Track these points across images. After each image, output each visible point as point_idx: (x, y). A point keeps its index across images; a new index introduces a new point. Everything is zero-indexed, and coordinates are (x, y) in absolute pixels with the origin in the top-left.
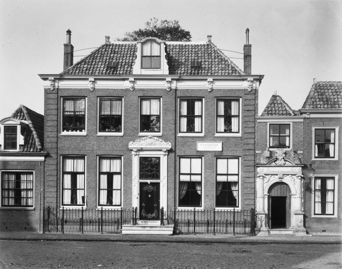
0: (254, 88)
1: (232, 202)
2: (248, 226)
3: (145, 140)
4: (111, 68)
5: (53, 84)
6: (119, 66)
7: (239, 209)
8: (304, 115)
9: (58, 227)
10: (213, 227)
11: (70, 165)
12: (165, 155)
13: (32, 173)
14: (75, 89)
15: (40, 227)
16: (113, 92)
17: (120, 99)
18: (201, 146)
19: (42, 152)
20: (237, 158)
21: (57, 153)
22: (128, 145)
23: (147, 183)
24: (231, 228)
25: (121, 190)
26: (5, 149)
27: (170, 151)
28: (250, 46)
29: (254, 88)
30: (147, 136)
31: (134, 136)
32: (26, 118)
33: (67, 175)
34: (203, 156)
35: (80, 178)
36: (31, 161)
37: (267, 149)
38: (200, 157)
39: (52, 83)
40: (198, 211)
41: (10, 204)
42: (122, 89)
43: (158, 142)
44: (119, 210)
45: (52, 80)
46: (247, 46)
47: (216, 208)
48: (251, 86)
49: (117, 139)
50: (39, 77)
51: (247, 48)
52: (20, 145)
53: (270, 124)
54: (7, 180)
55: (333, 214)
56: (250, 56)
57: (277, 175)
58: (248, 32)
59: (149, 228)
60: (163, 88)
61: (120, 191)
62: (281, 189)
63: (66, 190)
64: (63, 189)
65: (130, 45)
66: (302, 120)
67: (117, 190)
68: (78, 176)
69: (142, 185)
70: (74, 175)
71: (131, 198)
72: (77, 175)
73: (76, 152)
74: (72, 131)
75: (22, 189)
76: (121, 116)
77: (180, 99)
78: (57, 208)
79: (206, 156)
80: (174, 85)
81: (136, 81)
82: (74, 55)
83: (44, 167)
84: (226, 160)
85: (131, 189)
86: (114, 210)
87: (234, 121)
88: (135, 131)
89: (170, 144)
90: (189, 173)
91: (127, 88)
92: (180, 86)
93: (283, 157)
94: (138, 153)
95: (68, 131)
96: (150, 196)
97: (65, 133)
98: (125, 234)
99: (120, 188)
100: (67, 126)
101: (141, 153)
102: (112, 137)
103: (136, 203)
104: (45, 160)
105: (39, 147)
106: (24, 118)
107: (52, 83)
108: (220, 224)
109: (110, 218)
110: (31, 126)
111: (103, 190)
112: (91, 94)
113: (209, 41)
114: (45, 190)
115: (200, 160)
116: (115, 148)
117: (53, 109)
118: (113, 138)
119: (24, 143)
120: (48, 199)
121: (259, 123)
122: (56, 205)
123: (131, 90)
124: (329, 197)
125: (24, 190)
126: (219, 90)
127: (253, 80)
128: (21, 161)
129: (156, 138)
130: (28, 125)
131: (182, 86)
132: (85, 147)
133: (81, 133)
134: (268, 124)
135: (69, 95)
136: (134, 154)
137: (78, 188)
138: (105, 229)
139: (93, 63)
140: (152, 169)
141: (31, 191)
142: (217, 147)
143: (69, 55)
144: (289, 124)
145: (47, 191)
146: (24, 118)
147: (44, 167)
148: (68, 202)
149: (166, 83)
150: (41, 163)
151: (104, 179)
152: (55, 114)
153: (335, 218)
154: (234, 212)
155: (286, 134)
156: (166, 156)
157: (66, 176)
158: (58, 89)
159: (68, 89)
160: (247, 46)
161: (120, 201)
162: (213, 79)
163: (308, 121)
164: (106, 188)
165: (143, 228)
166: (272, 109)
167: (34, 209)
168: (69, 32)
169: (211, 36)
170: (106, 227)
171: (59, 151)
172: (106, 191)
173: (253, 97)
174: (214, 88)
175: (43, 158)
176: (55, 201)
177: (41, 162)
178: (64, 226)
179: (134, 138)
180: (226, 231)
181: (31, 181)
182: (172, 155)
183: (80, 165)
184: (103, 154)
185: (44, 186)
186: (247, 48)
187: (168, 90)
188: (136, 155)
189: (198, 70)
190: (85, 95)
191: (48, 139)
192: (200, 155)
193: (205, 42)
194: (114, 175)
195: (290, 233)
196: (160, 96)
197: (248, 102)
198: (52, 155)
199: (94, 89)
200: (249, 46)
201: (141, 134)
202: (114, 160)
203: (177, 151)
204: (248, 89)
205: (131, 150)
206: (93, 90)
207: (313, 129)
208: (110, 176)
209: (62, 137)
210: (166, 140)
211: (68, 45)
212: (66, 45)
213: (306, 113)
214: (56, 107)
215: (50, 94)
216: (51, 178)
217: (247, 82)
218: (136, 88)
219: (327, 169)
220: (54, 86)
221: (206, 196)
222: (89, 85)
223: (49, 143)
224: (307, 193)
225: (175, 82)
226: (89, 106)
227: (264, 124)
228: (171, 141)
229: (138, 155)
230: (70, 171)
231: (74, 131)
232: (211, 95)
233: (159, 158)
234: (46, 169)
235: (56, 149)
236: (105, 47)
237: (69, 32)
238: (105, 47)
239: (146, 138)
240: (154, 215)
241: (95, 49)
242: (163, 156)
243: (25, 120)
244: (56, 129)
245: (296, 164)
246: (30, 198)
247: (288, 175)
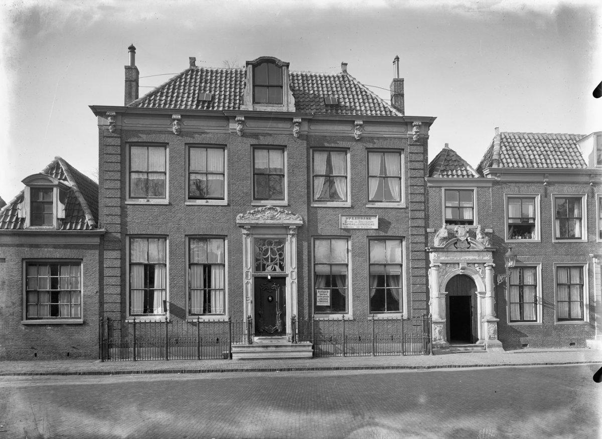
1: (394, 305)
4: (204, 102)
6: (217, 100)
7: (349, 316)
18: (354, 223)
26: (32, 224)
28: (402, 80)
31: (244, 204)
32: (66, 178)
37: (444, 226)
38: (347, 238)
40: (140, 323)
46: (398, 81)
49: (218, 210)
50: (91, 112)
51: (399, 83)
56: (403, 95)
58: (398, 61)
59: (274, 349)
65: (229, 72)
69: (256, 279)
81: (246, 121)
82: (139, 85)
93: (466, 238)
103: (248, 309)
105: (90, 223)
106: (63, 178)
110: (75, 188)
113: (343, 72)
119: (66, 216)
130: (70, 188)
136: (244, 234)
139: (175, 95)
140: (273, 255)
143: (134, 83)
144: (189, 198)
146: (63, 178)
151: (199, 271)
153: (539, 326)
155: (51, 278)
160: (398, 81)
166: (446, 168)
168: (132, 49)
170: (189, 348)
173: (421, 149)
183: (154, 251)
186: (399, 83)
189: (337, 110)
190: (166, 141)
192: (346, 235)
193: (337, 71)
197: (414, 157)
200: (400, 81)
211: (132, 69)
212: (127, 68)
219: (527, 255)
221: (356, 297)
227: (438, 190)
229: (252, 234)
236: (190, 73)
237: (132, 49)
238: (190, 73)
241: (175, 75)
243: (65, 179)
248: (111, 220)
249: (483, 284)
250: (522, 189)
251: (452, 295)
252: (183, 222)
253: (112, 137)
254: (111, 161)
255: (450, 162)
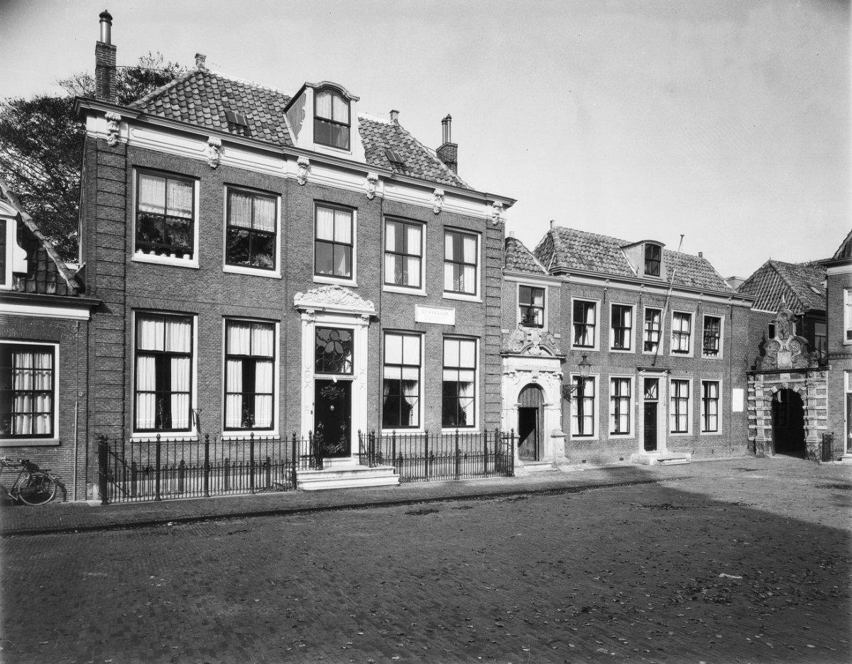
0: (124, 141)
2: (122, 476)
3: (327, 292)
5: (116, 131)
8: (563, 277)
9: (124, 485)
10: (155, 481)
11: (152, 335)
12: (364, 326)
13: (50, 351)
14: (171, 156)
15: (76, 489)
16: (260, 180)
17: (272, 195)
18: (424, 314)
19: (82, 297)
20: (473, 339)
21: (124, 304)
22: (292, 300)
23: (332, 381)
24: (200, 479)
25: (273, 394)
27: (373, 319)
29: (122, 139)
30: (329, 284)
33: (145, 358)
34: (424, 333)
35: (262, 370)
36: (51, 319)
38: (418, 334)
39: (114, 128)
41: (39, 432)
42: (279, 178)
43: (350, 299)
44: (151, 440)
45: (115, 120)
47: (444, 430)
48: (117, 134)
49: (269, 284)
52: (16, 275)
53: (520, 286)
54: (31, 367)
55: (592, 435)
57: (530, 371)
59: (350, 474)
60: (360, 190)
61: (187, 396)
62: (531, 395)
63: (143, 396)
64: (136, 392)
66: (559, 284)
67: (237, 393)
68: (174, 361)
69: (319, 384)
70: (163, 360)
71: (298, 413)
72: (172, 359)
73: (175, 306)
74: (158, 253)
75: (18, 391)
76: (274, 235)
77: (228, 188)
78: (123, 439)
79: (429, 333)
80: (382, 189)
83: (88, 335)
84: (457, 342)
85: (298, 393)
86: (271, 438)
87: (413, 265)
88: (307, 271)
89: (372, 304)
90: (401, 363)
91: (291, 176)
92: (389, 194)
94: (314, 319)
95: (146, 251)
96: (332, 407)
97: (139, 256)
98: (316, 489)
99: (187, 390)
100: (144, 240)
101: (319, 318)
102: (257, 279)
103: (307, 424)
104: (90, 319)
107: (114, 128)
108: (173, 469)
109: (413, 451)
111: (144, 395)
112: (210, 175)
114: (91, 394)
115: (418, 339)
116: (264, 304)
117: (114, 192)
118: (259, 280)
120: (98, 416)
121: (506, 281)
122: (120, 431)
123: (301, 182)
124: (587, 405)
125: (22, 393)
126: (450, 214)
127: (119, 118)
128: (16, 317)
129: (347, 291)
131: (246, 163)
132: (196, 296)
133: (168, 258)
134: (518, 284)
135: (156, 167)
136: (306, 320)
137: (174, 389)
138: (188, 484)
141: (44, 397)
142: (446, 317)
144: (544, 289)
145: (97, 395)
147: (88, 335)
148: (148, 422)
149: (368, 182)
150: (79, 323)
151: (236, 369)
152: (119, 205)
154: (158, 444)
156: (366, 328)
157: (142, 361)
158: (127, 145)
159: (154, 152)
161: (270, 419)
162: (380, 177)
163: (566, 286)
164: (240, 391)
165: (340, 475)
167: (61, 444)
168: (106, 17)
169: (397, 112)
171: (128, 299)
172: (240, 397)
174: (443, 209)
175: (84, 314)
176: (119, 422)
177: (80, 321)
178: (210, 478)
179: (306, 285)
180: (181, 487)
181: (43, 370)
182: (375, 326)
183: (179, 337)
184: (237, 315)
185: (87, 383)
187: (370, 196)
188: (309, 322)
191: (99, 265)
194: (258, 362)
195: (548, 467)
196: (354, 205)
198: (109, 306)
199: (218, 165)
200: (454, 146)
201: (317, 279)
202: (172, 324)
203: (383, 320)
204: (108, 138)
205: (301, 311)
206: (214, 166)
207: (572, 299)
208: (249, 364)
209: (137, 265)
210: (365, 296)
213: (605, 279)
214: (123, 189)
215: (104, 155)
216: (108, 365)
217: (105, 121)
218: (222, 162)
220: (117, 137)
222: (208, 154)
223: (104, 276)
224: (565, 401)
225: (381, 183)
226: (203, 202)
227: (513, 284)
228: (374, 298)
229: (315, 322)
230: (151, 348)
231: (152, 252)
232: (438, 221)
233: (351, 332)
234: (92, 341)
235: (122, 293)
239: (329, 287)
240: (338, 447)
242: (361, 327)
244: (122, 243)
245: (557, 355)
246: (40, 414)
247: (544, 372)
248: (109, 285)
249: (552, 393)
250: (586, 292)
251: (521, 406)
252: (220, 295)
253: (112, 153)
254: (109, 191)
255: (520, 253)
